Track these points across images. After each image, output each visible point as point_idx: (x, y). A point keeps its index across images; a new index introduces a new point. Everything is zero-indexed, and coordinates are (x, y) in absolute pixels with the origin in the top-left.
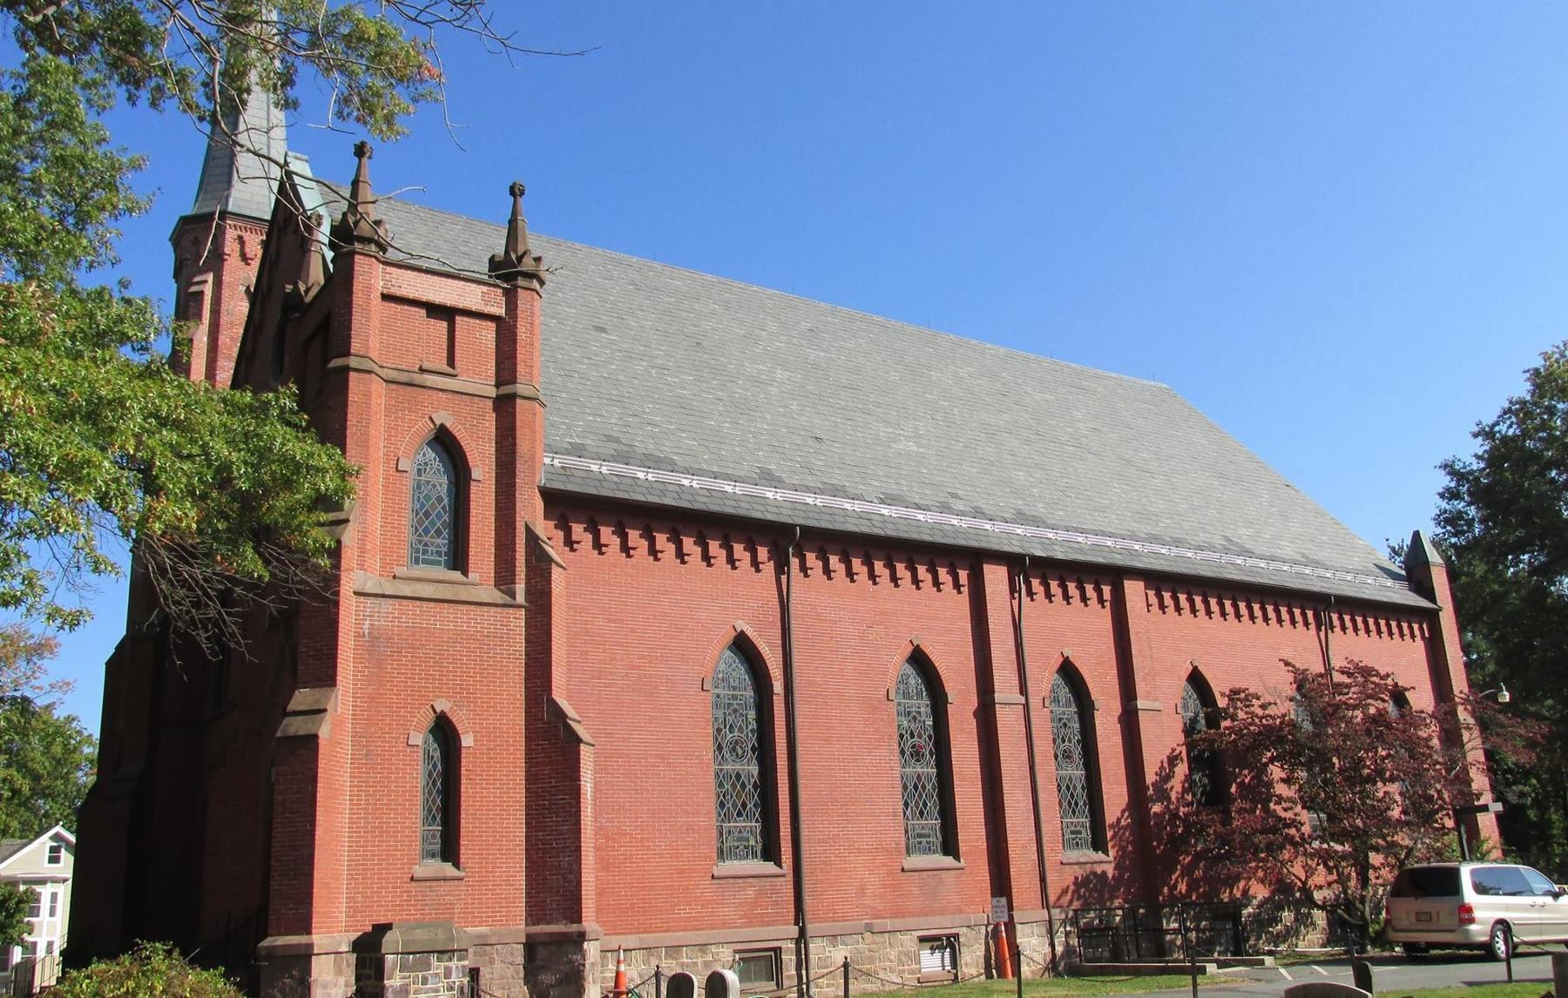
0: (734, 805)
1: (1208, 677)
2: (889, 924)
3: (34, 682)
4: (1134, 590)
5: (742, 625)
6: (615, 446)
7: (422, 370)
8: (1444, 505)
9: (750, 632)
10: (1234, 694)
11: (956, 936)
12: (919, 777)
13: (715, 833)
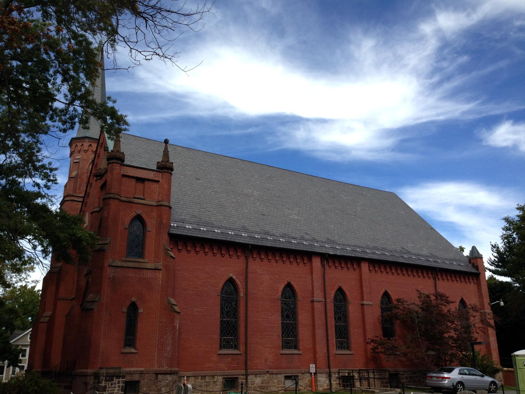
0: (226, 332)
1: (390, 294)
2: (275, 371)
3: (26, 280)
4: (365, 267)
5: (231, 275)
6: (195, 219)
7: (134, 198)
8: (504, 232)
9: (234, 277)
10: (398, 300)
11: (297, 376)
12: (288, 324)
13: (219, 340)
